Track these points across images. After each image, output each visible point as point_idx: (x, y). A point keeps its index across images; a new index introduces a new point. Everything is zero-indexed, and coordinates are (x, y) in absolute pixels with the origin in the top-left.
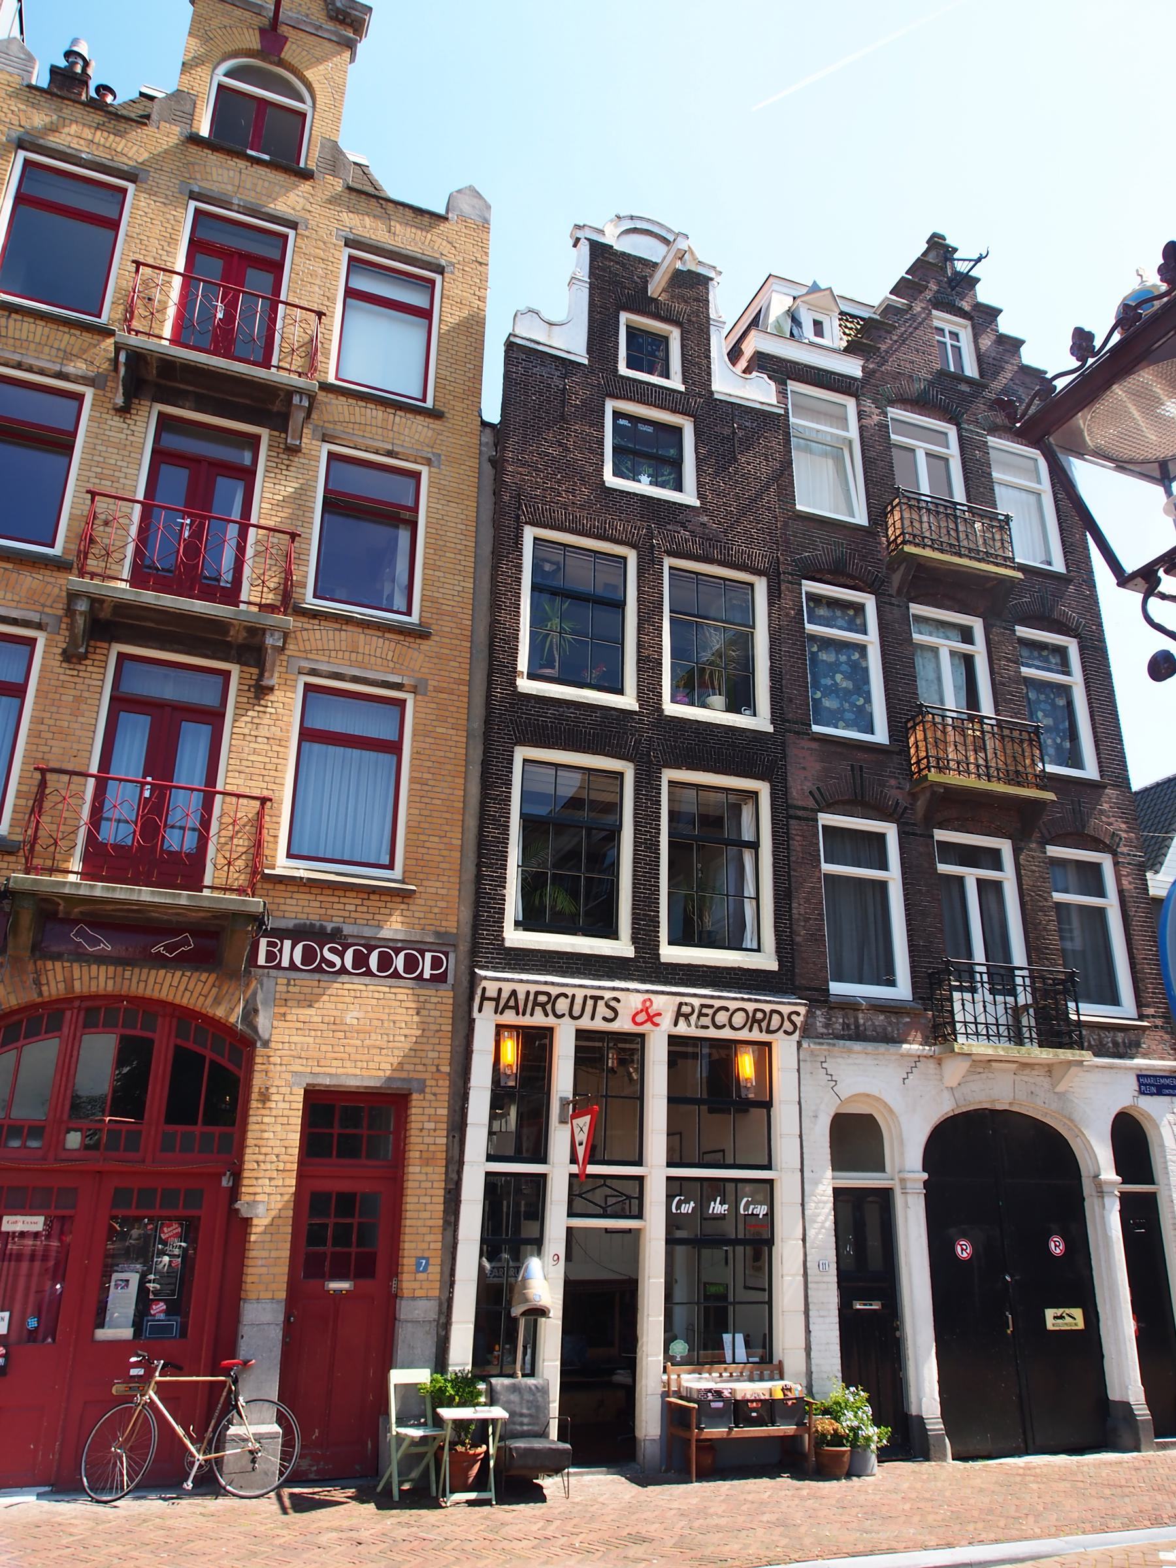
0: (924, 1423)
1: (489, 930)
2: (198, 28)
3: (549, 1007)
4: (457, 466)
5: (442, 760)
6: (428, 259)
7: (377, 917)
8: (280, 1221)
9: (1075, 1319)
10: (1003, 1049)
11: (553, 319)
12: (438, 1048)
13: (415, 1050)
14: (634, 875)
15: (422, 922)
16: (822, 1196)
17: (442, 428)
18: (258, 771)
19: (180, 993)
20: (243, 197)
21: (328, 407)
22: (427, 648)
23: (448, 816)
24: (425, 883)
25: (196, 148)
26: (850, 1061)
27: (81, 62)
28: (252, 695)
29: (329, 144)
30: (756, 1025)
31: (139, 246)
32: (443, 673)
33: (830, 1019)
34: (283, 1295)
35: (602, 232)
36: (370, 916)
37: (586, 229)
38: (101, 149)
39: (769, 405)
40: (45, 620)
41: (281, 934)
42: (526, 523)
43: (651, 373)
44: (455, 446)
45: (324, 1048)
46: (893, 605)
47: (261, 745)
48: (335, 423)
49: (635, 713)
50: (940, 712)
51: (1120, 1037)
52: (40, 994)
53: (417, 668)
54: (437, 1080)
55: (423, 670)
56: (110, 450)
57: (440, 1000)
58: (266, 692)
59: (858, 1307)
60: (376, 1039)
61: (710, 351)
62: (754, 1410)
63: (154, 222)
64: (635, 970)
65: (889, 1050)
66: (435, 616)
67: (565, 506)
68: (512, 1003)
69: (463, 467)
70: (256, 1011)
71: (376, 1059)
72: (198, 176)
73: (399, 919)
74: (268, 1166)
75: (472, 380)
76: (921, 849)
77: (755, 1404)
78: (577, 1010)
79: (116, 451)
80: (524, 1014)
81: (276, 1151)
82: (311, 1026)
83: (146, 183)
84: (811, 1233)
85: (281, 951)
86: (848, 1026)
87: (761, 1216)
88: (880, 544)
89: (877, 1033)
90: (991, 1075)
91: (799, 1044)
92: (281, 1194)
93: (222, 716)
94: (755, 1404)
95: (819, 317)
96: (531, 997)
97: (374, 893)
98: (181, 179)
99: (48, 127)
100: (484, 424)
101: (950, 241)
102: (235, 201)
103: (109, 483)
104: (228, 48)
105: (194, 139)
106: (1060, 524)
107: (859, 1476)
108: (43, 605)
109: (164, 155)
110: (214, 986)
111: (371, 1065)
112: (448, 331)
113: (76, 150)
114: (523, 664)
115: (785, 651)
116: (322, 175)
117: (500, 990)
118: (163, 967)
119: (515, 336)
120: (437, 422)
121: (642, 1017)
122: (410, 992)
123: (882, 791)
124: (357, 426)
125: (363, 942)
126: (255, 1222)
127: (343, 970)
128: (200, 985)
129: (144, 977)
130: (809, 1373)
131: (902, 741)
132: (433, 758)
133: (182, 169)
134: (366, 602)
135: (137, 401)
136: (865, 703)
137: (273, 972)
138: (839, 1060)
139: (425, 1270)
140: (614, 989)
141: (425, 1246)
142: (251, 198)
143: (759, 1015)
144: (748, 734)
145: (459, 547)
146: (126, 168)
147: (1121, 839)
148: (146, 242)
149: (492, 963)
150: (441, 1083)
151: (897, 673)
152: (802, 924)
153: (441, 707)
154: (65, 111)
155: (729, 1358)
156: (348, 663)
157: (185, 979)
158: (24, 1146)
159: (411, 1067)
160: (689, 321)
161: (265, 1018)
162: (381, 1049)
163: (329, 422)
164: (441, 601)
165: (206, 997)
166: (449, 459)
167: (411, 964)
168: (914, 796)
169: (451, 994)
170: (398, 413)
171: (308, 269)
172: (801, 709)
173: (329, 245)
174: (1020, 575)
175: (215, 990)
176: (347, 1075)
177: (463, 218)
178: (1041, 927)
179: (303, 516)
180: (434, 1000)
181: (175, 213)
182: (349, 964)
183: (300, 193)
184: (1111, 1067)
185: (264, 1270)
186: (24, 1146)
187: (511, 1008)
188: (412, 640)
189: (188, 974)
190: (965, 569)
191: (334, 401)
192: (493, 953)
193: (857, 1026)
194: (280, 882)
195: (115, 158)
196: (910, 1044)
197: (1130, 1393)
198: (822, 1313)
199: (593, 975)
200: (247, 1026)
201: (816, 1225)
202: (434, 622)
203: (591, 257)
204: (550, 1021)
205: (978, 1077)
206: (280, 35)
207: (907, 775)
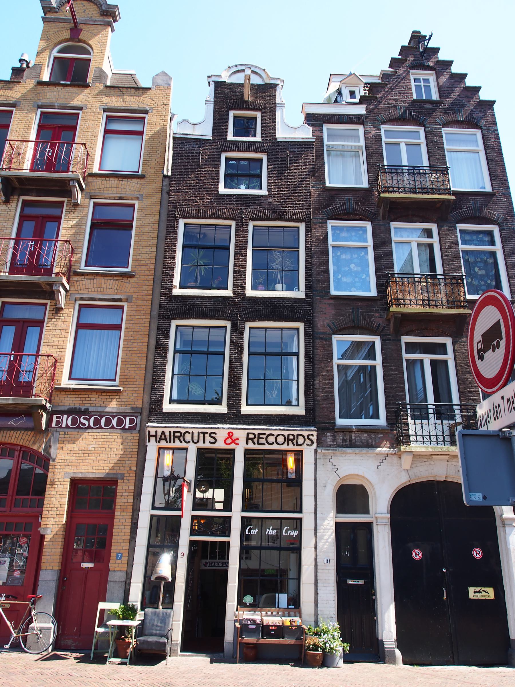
0: (384, 644)
1: (156, 405)
2: (45, 36)
3: (181, 438)
4: (151, 198)
5: (137, 330)
6: (141, 109)
7: (105, 403)
8: (56, 536)
9: (490, 593)
10: (432, 448)
11: (195, 122)
13: (120, 461)
14: (229, 374)
15: (125, 403)
16: (327, 526)
17: (144, 182)
18: (55, 344)
19: (19, 440)
20: (59, 102)
21: (92, 183)
22: (133, 281)
24: (128, 386)
25: (41, 86)
26: (346, 458)
27: (25, 63)
28: (54, 312)
30: (290, 442)
31: (16, 133)
32: (140, 291)
33: (335, 437)
35: (220, 76)
39: (307, 138)
41: (63, 413)
42: (180, 218)
43: (248, 136)
44: (150, 189)
45: (79, 461)
46: (381, 225)
47: (58, 333)
48: (95, 190)
49: (231, 297)
50: (412, 276)
55: (130, 291)
57: (132, 437)
58: (60, 310)
59: (351, 583)
60: (103, 456)
61: (275, 119)
62: (273, 630)
63: (22, 122)
64: (228, 419)
65: (368, 451)
66: (137, 267)
67: (199, 207)
68: (163, 437)
70: (50, 446)
71: (102, 465)
72: (41, 98)
73: (115, 403)
74: (53, 513)
76: (393, 347)
77: (273, 628)
80: (170, 442)
81: (56, 506)
82: (74, 452)
84: (320, 545)
85: (62, 420)
86: (346, 440)
87: (294, 536)
88: (374, 195)
89: (363, 443)
90: (432, 463)
91: (316, 451)
92: (58, 525)
93: (44, 322)
94: (273, 628)
95: (352, 89)
96: (172, 434)
97: (104, 392)
100: (165, 177)
102: (56, 105)
104: (56, 41)
105: (41, 83)
106: (488, 166)
107: (328, 667)
109: (28, 93)
111: (100, 468)
112: (149, 138)
114: (176, 281)
116: (94, 84)
117: (156, 432)
119: (175, 134)
120: (142, 180)
121: (229, 441)
122: (119, 435)
123: (370, 320)
124: (105, 189)
126: (46, 536)
127: (89, 427)
129: (4, 435)
130: (316, 615)
131: (384, 293)
132: (133, 330)
134: (114, 265)
135: (12, 197)
136: (366, 277)
137: (58, 430)
138: (340, 458)
139: (120, 559)
140: (211, 428)
141: (121, 548)
142: (62, 102)
143: (291, 437)
144: (291, 300)
146: (12, 102)
148: (19, 131)
149: (157, 420)
150: (131, 475)
151: (381, 259)
152: (321, 391)
153: (139, 307)
155: (277, 606)
156: (97, 293)
157: (21, 434)
160: (265, 107)
161: (54, 449)
162: (105, 460)
163: (93, 190)
165: (30, 441)
166: (146, 195)
167: (120, 422)
168: (389, 320)
169: (138, 435)
170: (124, 180)
171: (87, 126)
172: (324, 284)
174: (453, 197)
175: (33, 438)
176: (89, 472)
177: (158, 87)
178: (467, 382)
179: (80, 232)
181: (31, 116)
183: (84, 94)
185: (49, 557)
187: (163, 439)
188: (126, 279)
189: (23, 432)
190: (414, 200)
191: (95, 180)
192: (157, 415)
193: (351, 440)
194: (63, 391)
195: (8, 100)
196: (382, 448)
198: (325, 585)
199: (206, 422)
200: (46, 453)
201: (323, 541)
202: (137, 269)
204: (184, 445)
205: (424, 463)
206: (79, 29)
207: (385, 310)
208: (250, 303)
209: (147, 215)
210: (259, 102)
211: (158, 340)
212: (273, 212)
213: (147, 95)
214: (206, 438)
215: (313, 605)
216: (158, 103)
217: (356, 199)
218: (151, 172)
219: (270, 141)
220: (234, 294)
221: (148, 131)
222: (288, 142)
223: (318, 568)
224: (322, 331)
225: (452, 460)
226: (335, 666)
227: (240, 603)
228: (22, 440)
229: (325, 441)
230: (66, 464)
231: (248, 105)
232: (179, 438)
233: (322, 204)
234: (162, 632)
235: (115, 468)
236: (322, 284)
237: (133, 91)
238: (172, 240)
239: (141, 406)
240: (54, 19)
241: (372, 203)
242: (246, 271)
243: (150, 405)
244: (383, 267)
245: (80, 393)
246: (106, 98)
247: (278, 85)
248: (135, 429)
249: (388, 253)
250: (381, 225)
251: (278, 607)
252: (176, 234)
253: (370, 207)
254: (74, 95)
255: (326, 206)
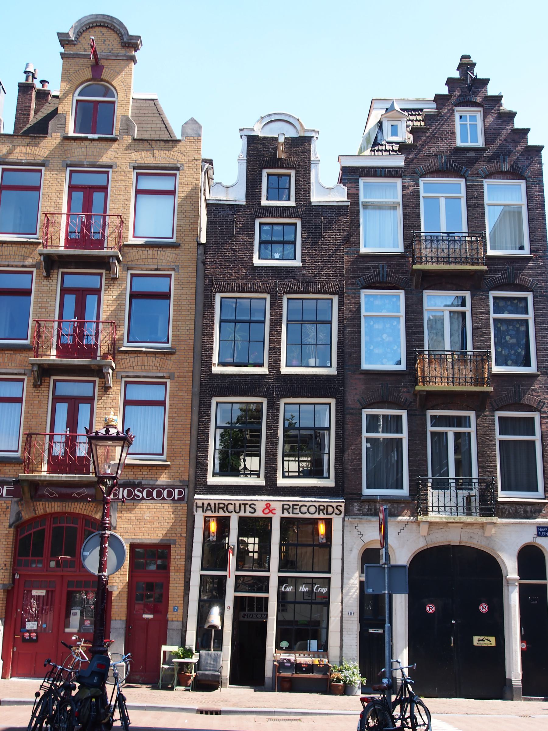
3: (225, 509)
4: (186, 269)
7: (155, 476)
8: (122, 593)
9: (492, 641)
12: (181, 527)
15: (174, 477)
23: (184, 431)
24: (175, 461)
26: (371, 525)
29: (125, 118)
32: (181, 369)
33: (361, 507)
34: (125, 618)
35: (252, 130)
36: (153, 476)
37: (245, 130)
38: (30, 155)
39: (341, 202)
40: (26, 372)
42: (216, 292)
44: (185, 259)
45: (136, 529)
46: (413, 294)
48: (132, 261)
49: (267, 375)
51: (529, 508)
52: (36, 514)
53: (170, 368)
54: (181, 540)
56: (44, 295)
60: (156, 524)
61: (310, 179)
62: (304, 667)
67: (234, 280)
68: (209, 508)
69: (189, 269)
71: (156, 532)
72: (69, 156)
73: (165, 476)
75: (193, 224)
77: (305, 665)
78: (237, 509)
79: (46, 295)
80: (215, 512)
83: (49, 166)
84: (345, 600)
85: (119, 492)
90: (448, 530)
96: (217, 505)
98: (62, 159)
99: (9, 152)
100: (199, 244)
101: (473, 59)
102: (85, 163)
103: (45, 310)
108: (25, 366)
110: (95, 507)
112: (182, 201)
113: (20, 159)
115: (349, 331)
116: (122, 136)
117: (203, 504)
118: (76, 501)
120: (177, 249)
121: (267, 511)
124: (141, 260)
125: (150, 487)
126: (113, 593)
127: (143, 498)
128: (90, 507)
129: (70, 506)
130: (341, 657)
132: (177, 407)
133: (63, 155)
138: (365, 525)
139: (177, 611)
140: (251, 500)
141: (177, 602)
142: (91, 160)
143: (322, 508)
145: (188, 308)
147: (544, 403)
150: (182, 540)
151: (412, 332)
154: (14, 142)
157: (84, 506)
158: (37, 566)
159: (170, 535)
160: (299, 165)
162: (158, 528)
163: (130, 261)
164: (180, 336)
165: (92, 512)
167: (170, 494)
169: (186, 505)
170: (160, 249)
172: (356, 359)
173: (126, 173)
175: (95, 509)
178: (486, 455)
180: (179, 508)
182: (145, 496)
183: (113, 150)
184: (521, 523)
185: (117, 610)
186: (37, 566)
188: (168, 356)
189: (85, 503)
191: (131, 251)
197: (512, 675)
198: (349, 633)
199: (246, 494)
201: (348, 597)
203: (247, 145)
204: (227, 514)
205: (440, 530)
208: (285, 380)
209: (184, 288)
210: (293, 159)
211: (200, 417)
212: (307, 285)
213: (177, 149)
214: (247, 508)
215: (339, 649)
216: (189, 158)
217: (390, 266)
218: (186, 240)
219: (304, 206)
220: (269, 371)
221: (180, 193)
222: (323, 206)
223: (344, 619)
224: (352, 406)
225: (466, 527)
226: (354, 694)
227: (278, 647)
228: (86, 511)
229: (353, 510)
230: (125, 531)
231: (282, 163)
232: (223, 508)
233: (356, 272)
234: (215, 669)
235: (168, 535)
236: (353, 359)
237: (162, 143)
238: (209, 316)
239: (187, 479)
240: (73, 54)
241: (406, 271)
242: (281, 347)
243: (196, 478)
244: (413, 340)
245: (160, 468)
246: (135, 153)
247: (313, 137)
248: (184, 500)
249: (419, 325)
250: (413, 294)
251: (310, 651)
252: (213, 310)
253: (404, 275)
254: (103, 150)
255: (360, 275)
